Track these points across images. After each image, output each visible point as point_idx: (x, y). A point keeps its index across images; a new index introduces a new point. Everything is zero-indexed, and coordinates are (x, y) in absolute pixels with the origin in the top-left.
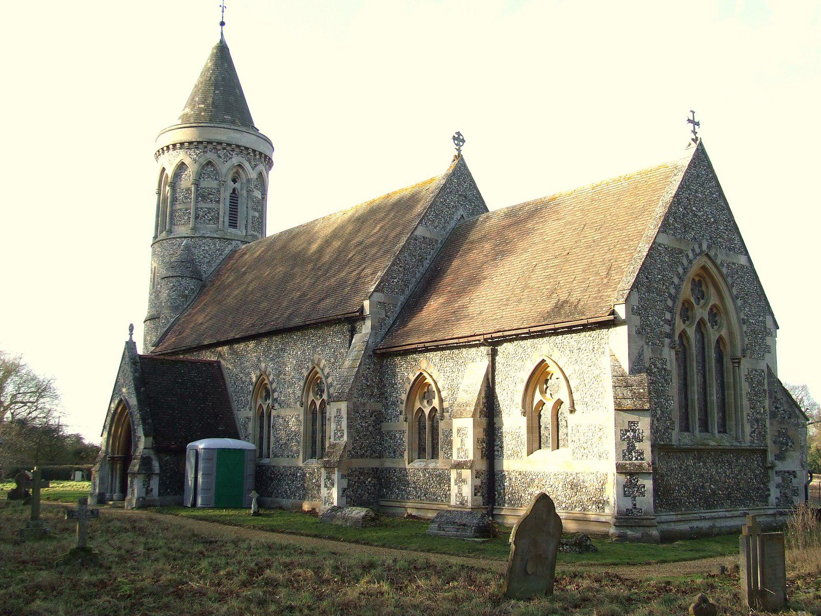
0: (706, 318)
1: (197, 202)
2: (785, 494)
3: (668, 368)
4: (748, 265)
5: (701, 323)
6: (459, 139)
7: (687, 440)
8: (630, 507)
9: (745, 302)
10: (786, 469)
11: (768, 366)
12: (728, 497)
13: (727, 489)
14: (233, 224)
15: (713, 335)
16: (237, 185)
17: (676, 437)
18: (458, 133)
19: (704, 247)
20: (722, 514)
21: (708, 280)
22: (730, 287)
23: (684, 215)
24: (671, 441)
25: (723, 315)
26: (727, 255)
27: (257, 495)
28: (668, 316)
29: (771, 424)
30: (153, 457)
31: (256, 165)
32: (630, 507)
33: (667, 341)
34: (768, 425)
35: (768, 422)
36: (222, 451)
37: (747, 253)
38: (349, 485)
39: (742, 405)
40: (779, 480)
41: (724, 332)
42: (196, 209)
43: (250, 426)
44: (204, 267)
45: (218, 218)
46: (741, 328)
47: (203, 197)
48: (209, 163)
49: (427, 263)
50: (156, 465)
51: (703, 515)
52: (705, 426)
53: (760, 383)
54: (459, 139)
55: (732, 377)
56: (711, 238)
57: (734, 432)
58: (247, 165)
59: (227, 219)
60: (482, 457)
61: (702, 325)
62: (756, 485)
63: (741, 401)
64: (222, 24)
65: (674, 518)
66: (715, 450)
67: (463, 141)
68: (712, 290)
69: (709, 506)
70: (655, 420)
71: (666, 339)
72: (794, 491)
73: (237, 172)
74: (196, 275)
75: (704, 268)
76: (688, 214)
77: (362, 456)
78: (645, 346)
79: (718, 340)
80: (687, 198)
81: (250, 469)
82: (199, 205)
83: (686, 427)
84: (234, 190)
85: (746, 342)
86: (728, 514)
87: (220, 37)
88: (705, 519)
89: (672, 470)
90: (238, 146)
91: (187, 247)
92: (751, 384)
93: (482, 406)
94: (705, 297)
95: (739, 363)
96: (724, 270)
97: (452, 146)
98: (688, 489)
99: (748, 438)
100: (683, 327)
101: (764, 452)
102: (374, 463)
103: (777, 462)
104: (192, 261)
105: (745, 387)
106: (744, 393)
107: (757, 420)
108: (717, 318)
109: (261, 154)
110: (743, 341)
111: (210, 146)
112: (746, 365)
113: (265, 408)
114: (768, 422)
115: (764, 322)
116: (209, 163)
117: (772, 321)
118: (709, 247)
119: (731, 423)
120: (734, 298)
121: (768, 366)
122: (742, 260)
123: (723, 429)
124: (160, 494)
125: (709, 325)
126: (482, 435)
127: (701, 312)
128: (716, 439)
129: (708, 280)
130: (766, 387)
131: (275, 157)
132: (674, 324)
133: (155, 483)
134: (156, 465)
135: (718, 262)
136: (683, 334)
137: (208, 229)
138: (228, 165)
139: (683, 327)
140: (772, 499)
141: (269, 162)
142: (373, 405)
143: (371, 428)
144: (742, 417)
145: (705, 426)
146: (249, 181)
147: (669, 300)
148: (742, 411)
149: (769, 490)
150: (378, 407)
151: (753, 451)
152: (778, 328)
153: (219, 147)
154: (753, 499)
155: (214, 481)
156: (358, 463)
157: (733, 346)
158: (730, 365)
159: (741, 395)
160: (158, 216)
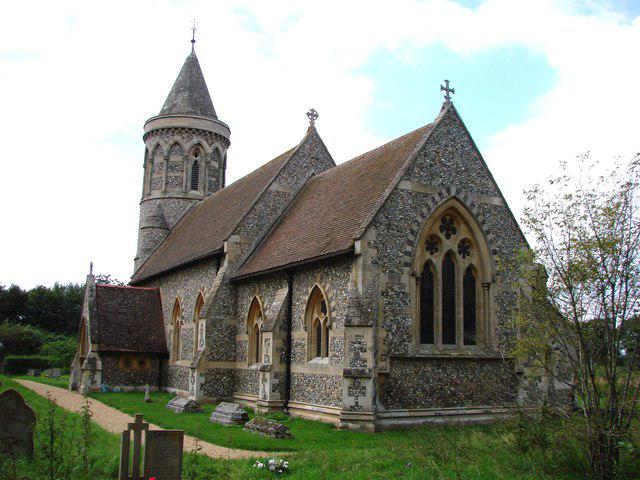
0: (455, 249)
3: (407, 290)
5: (449, 254)
6: (313, 115)
7: (426, 350)
8: (353, 404)
9: (498, 236)
12: (470, 397)
15: (462, 264)
17: (413, 348)
18: (313, 110)
19: (453, 192)
22: (480, 225)
23: (431, 165)
26: (480, 198)
37: (501, 196)
38: (206, 382)
41: (474, 261)
47: (172, 168)
48: (176, 143)
49: (279, 212)
50: (99, 364)
52: (449, 338)
53: (512, 303)
54: (313, 115)
58: (205, 143)
59: (189, 184)
65: (407, 414)
66: (456, 359)
67: (317, 116)
69: (447, 405)
73: (198, 149)
74: (165, 226)
77: (218, 360)
84: (196, 162)
87: (190, 51)
91: (160, 206)
96: (475, 211)
98: (424, 390)
104: (162, 216)
105: (494, 305)
109: (216, 134)
113: (322, 321)
116: (176, 143)
118: (458, 191)
119: (479, 336)
122: (496, 201)
123: (468, 342)
126: (280, 344)
127: (450, 244)
128: (460, 349)
131: (232, 139)
133: (98, 377)
134: (99, 364)
135: (468, 204)
136: (428, 264)
137: (176, 192)
141: (227, 143)
142: (228, 321)
145: (449, 338)
146: (206, 155)
153: (183, 131)
156: (214, 365)
157: (484, 272)
158: (481, 289)
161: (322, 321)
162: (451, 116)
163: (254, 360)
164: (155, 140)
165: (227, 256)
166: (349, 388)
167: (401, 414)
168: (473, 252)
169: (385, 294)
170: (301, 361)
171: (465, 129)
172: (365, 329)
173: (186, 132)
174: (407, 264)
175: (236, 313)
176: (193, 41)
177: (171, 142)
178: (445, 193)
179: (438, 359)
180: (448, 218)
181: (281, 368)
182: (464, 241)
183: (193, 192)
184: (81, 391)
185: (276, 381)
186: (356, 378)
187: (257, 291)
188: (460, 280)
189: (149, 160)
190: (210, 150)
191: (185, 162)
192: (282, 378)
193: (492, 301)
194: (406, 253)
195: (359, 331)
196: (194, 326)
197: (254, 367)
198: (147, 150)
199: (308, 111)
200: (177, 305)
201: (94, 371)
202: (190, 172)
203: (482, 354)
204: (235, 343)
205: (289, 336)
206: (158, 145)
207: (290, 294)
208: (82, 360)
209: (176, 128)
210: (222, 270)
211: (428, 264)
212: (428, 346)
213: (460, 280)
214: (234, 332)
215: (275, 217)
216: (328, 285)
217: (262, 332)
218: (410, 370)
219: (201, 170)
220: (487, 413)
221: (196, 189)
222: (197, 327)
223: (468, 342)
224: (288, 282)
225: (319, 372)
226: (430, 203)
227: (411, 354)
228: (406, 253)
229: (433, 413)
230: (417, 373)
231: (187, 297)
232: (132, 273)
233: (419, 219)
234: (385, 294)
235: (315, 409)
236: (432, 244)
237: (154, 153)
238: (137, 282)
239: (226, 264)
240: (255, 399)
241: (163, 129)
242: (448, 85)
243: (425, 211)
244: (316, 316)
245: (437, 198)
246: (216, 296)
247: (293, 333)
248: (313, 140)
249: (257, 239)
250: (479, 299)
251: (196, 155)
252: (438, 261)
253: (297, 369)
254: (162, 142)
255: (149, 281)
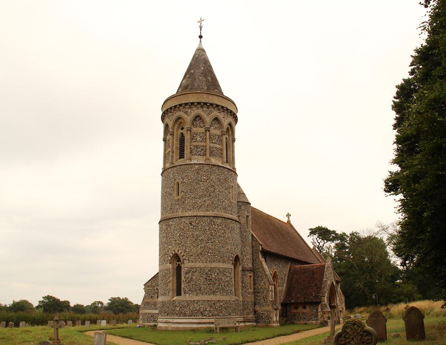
64: (201, 37)
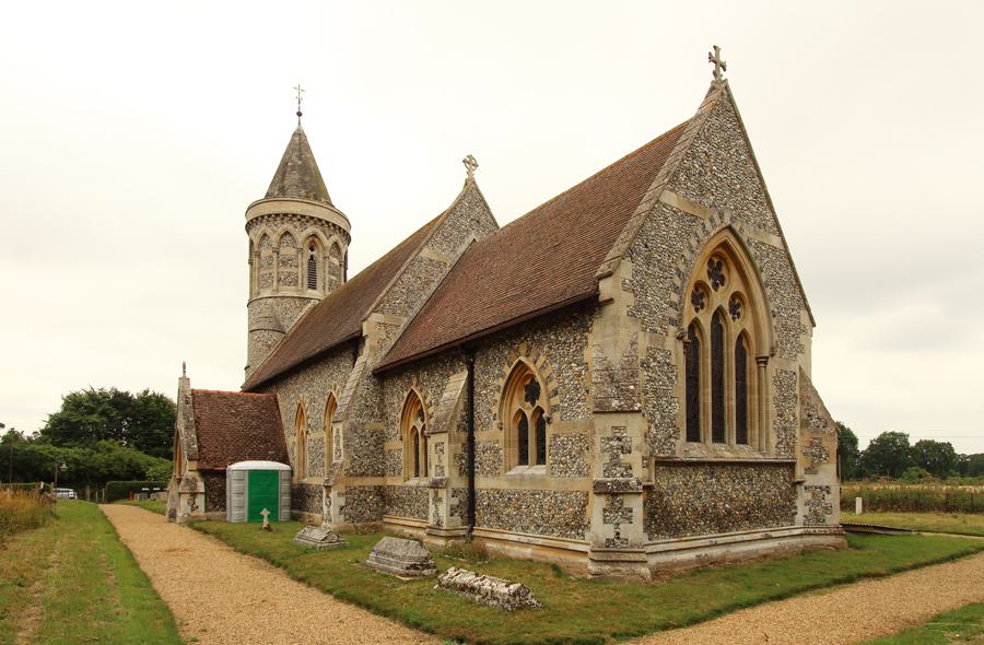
0: (726, 307)
1: (278, 266)
2: (815, 511)
4: (782, 248)
6: (470, 163)
7: (697, 452)
8: (612, 536)
9: (776, 291)
10: (819, 484)
11: (800, 368)
12: (747, 517)
13: (745, 508)
14: (312, 286)
15: (734, 328)
16: (314, 253)
17: (683, 449)
20: (738, 538)
21: (729, 260)
24: (674, 452)
25: (748, 305)
26: (756, 233)
27: (269, 513)
28: (675, 298)
29: (802, 434)
30: (198, 478)
31: (330, 236)
32: (612, 536)
33: (672, 329)
34: (797, 435)
35: (798, 430)
36: (253, 473)
38: (347, 504)
39: (767, 412)
40: (808, 496)
41: (749, 327)
42: (278, 273)
43: (295, 449)
44: (286, 323)
45: (297, 281)
46: (770, 321)
48: (287, 233)
49: (434, 286)
51: (714, 540)
52: (719, 436)
53: (791, 387)
55: (756, 380)
56: (736, 208)
57: (757, 443)
58: (321, 235)
59: (306, 281)
60: (460, 475)
61: (721, 317)
62: (782, 502)
63: (767, 405)
67: (476, 166)
68: (735, 274)
69: (722, 529)
70: (653, 426)
71: (671, 326)
72: (827, 508)
73: (313, 241)
75: (725, 245)
76: (706, 173)
77: (362, 475)
78: (641, 334)
79: (740, 336)
80: (705, 152)
81: (284, 487)
82: (280, 270)
83: (693, 435)
84: (312, 257)
85: (776, 338)
86: (746, 537)
88: (716, 545)
89: (674, 487)
90: (312, 218)
92: (780, 387)
93: (459, 418)
94: (726, 284)
95: (766, 363)
97: (463, 169)
99: (774, 450)
100: (695, 315)
101: (791, 466)
102: (377, 481)
103: (806, 476)
105: (772, 391)
106: (771, 397)
107: (785, 429)
108: (740, 310)
110: (772, 337)
111: (286, 219)
112: (773, 366)
114: (798, 430)
115: (799, 318)
117: (807, 317)
119: (753, 433)
120: (762, 286)
121: (800, 368)
122: (775, 241)
123: (742, 439)
124: (207, 510)
125: (730, 316)
127: (720, 298)
128: (727, 452)
129: (729, 260)
130: (797, 392)
132: (682, 308)
133: (200, 501)
134: (201, 487)
136: (695, 324)
138: (305, 233)
139: (695, 315)
140: (799, 518)
141: (348, 239)
142: (372, 424)
143: (371, 448)
144: (767, 424)
147: (676, 277)
148: (767, 418)
149: (796, 508)
150: (381, 426)
151: (775, 465)
152: (814, 325)
154: (777, 519)
155: (247, 499)
158: (755, 366)
159: (767, 400)
160: (251, 282)
161: (529, 414)
162: (721, 104)
163: (412, 473)
164: (262, 228)
165: (367, 341)
166: (605, 510)
167: (667, 547)
168: (745, 311)
169: (645, 365)
170: (493, 472)
171: (741, 126)
172: (629, 416)
173: (295, 210)
174: (672, 322)
175: (383, 415)
176: (299, 114)
177: (280, 230)
178: (718, 221)
179: (712, 464)
180: (716, 260)
181: (460, 483)
182: (736, 295)
183: (310, 291)
184: (178, 520)
185: (455, 501)
186: (614, 495)
187: (415, 382)
188: (730, 351)
189: (254, 252)
190: (328, 243)
191: (300, 256)
192: (463, 497)
193: (770, 383)
194: (672, 304)
195: (619, 420)
196: (325, 435)
197: (413, 482)
198: (251, 243)
199: (464, 157)
200: (300, 412)
201: (194, 495)
202: (306, 266)
203: (758, 457)
204: (383, 453)
205: (471, 441)
206: (265, 235)
207: (471, 379)
208: (179, 481)
209: (286, 215)
210: (360, 360)
211: (695, 324)
212: (695, 444)
213: (730, 351)
214: (381, 439)
215: (429, 292)
216: (542, 359)
217: (663, 346)
218: (678, 479)
219: (319, 266)
220: (768, 538)
221: (315, 288)
222: (330, 436)
223: (742, 439)
224: (467, 363)
225: (527, 487)
226: (700, 233)
227: (681, 457)
228: (672, 304)
229: (707, 542)
230: (686, 485)
231: (313, 400)
232: (244, 381)
233: (687, 254)
234: (645, 365)
235: (523, 539)
236: (699, 295)
237: (260, 245)
238: (254, 387)
239: (366, 350)
240: (424, 525)
241: (269, 216)
242: (717, 54)
243: (693, 242)
244: (517, 406)
245: (708, 225)
246: (355, 392)
247: (476, 434)
248: (472, 198)
249: (405, 320)
250: (752, 381)
251: (312, 250)
252: (706, 321)
253: (483, 483)
254: (269, 231)
255: (265, 384)
